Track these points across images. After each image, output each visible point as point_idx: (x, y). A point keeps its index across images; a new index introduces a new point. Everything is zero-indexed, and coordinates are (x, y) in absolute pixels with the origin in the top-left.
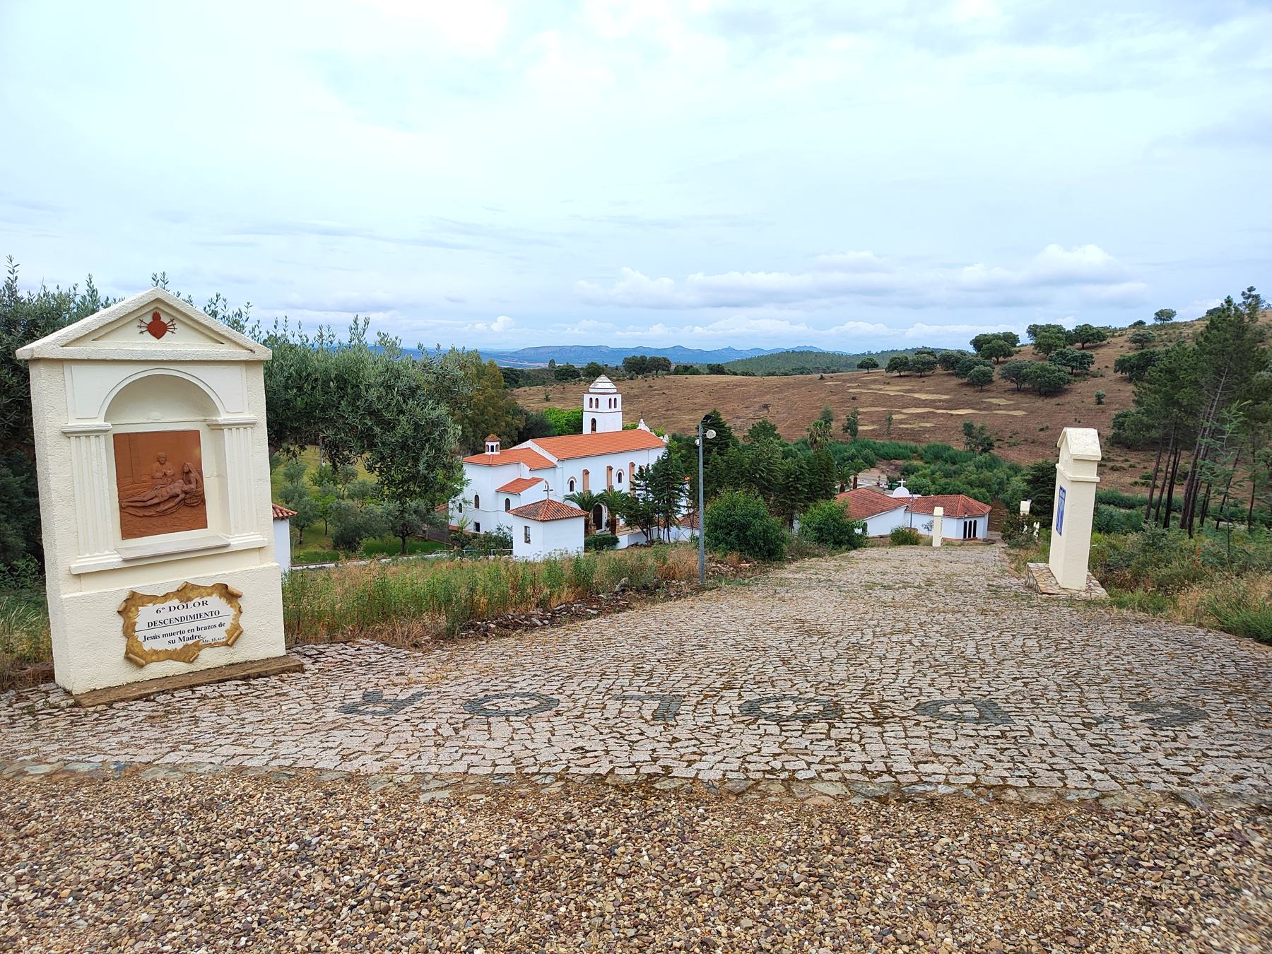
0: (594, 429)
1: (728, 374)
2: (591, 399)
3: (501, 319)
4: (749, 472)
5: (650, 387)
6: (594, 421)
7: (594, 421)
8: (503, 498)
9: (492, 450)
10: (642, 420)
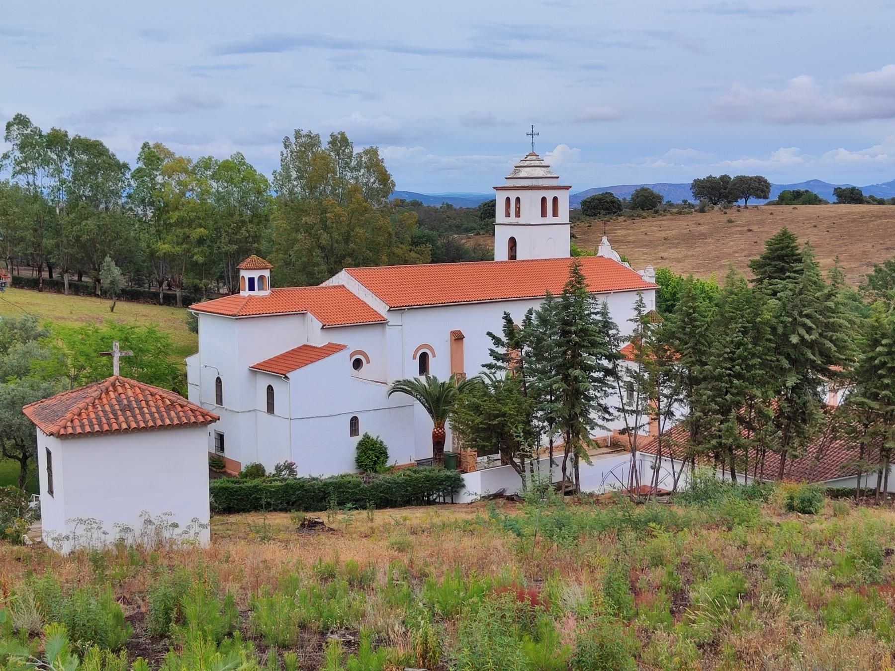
0: (513, 257)
1: (868, 203)
2: (508, 199)
3: (560, 147)
4: (774, 329)
5: (730, 221)
6: (513, 242)
7: (513, 242)
8: (263, 383)
9: (252, 288)
10: (605, 239)
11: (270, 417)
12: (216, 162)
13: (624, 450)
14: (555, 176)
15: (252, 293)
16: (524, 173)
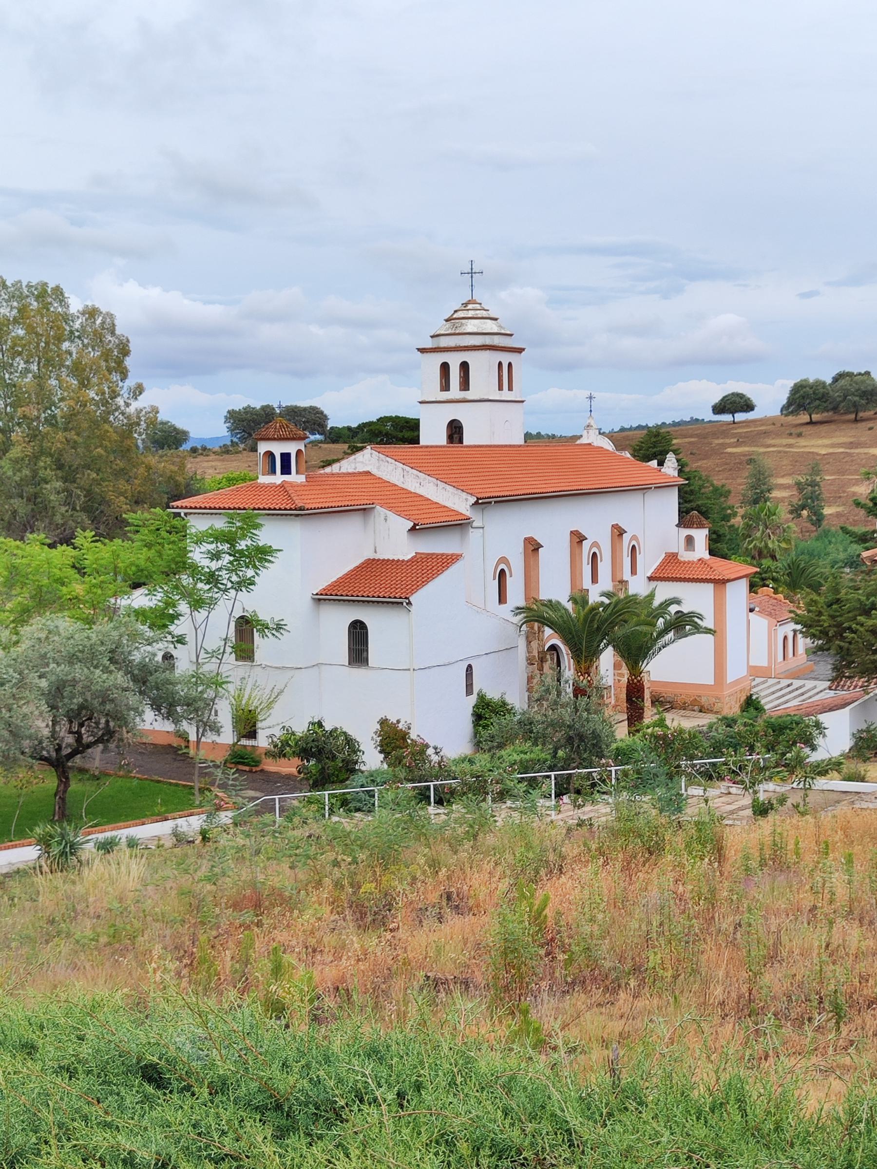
8: (347, 614)
11: (358, 673)
12: (29, 286)
13: (672, 708)
14: (508, 332)
15: (286, 478)
16: (471, 326)
